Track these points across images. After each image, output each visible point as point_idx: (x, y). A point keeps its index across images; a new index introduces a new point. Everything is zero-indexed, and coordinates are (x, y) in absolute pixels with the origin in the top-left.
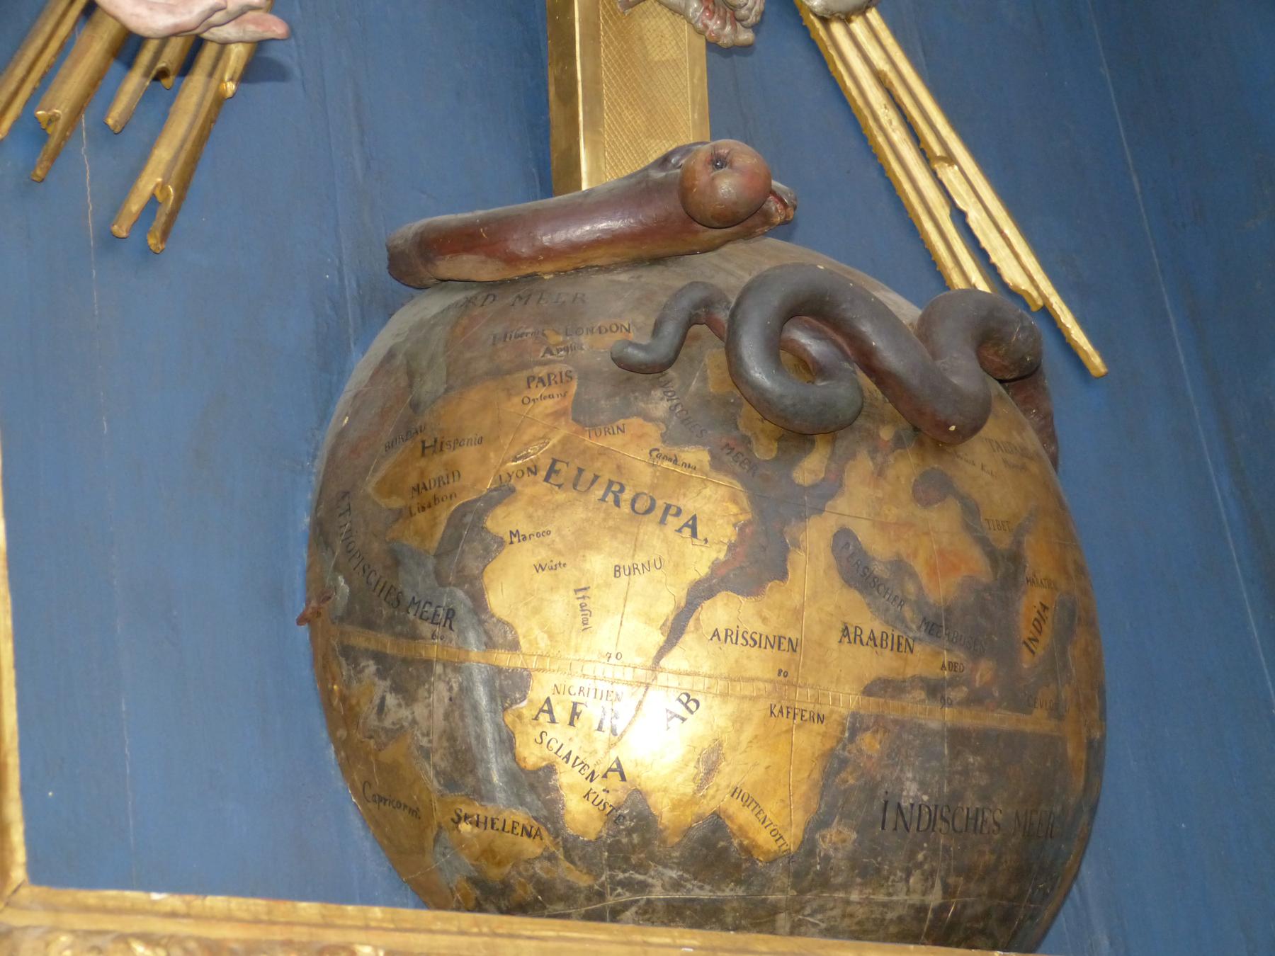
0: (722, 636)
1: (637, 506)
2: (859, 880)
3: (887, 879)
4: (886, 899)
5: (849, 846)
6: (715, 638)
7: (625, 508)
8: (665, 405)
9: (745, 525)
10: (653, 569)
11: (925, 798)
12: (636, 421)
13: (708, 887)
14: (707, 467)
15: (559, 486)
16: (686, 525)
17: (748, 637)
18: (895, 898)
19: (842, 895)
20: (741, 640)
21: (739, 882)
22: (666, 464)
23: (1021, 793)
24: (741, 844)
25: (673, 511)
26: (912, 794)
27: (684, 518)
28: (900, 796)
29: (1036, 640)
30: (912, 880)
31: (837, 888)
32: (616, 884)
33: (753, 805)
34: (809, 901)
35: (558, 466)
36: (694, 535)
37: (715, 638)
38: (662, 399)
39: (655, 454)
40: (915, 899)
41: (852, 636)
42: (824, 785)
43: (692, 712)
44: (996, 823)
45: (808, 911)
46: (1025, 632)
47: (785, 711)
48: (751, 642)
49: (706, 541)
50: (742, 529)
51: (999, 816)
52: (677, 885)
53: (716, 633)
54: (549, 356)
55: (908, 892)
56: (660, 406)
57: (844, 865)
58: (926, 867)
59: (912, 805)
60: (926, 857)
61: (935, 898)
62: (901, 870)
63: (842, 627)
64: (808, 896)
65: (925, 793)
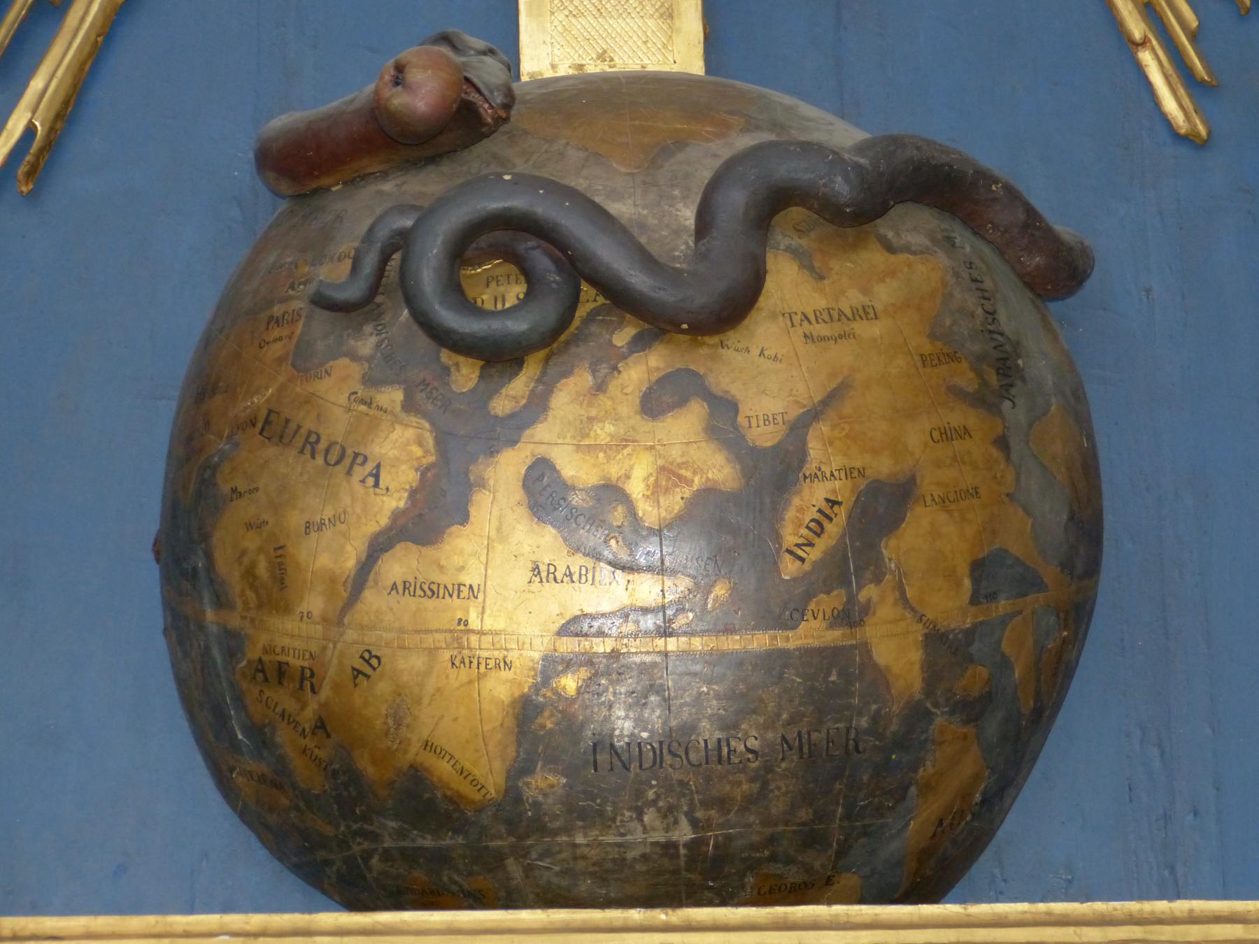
0: (401, 588)
1: (329, 457)
2: (580, 823)
3: (614, 820)
4: (619, 839)
5: (560, 791)
6: (394, 592)
7: (320, 460)
8: (373, 340)
9: (428, 469)
10: (338, 523)
11: (645, 735)
12: (343, 361)
13: (429, 837)
14: (398, 408)
15: (269, 439)
16: (371, 474)
17: (426, 587)
18: (629, 837)
19: (563, 839)
20: (419, 592)
21: (456, 831)
22: (363, 408)
23: (785, 716)
24: (445, 796)
25: (360, 460)
26: (626, 733)
27: (370, 467)
28: (612, 736)
29: (811, 544)
30: (646, 818)
31: (555, 833)
32: (355, 834)
33: (448, 757)
34: (532, 846)
35: (273, 417)
36: (376, 485)
37: (394, 592)
38: (371, 334)
39: (353, 397)
40: (660, 837)
41: (544, 574)
42: (520, 732)
43: (374, 669)
44: (749, 750)
45: (534, 855)
46: (790, 539)
47: (467, 661)
48: (429, 593)
49: (387, 489)
50: (423, 474)
51: (753, 743)
52: (401, 834)
53: (394, 587)
54: (291, 292)
55: (645, 830)
56: (367, 344)
57: (557, 809)
58: (661, 804)
59: (628, 744)
60: (658, 796)
61: (684, 833)
62: (629, 809)
63: (530, 565)
64: (529, 842)
65: (645, 730)
